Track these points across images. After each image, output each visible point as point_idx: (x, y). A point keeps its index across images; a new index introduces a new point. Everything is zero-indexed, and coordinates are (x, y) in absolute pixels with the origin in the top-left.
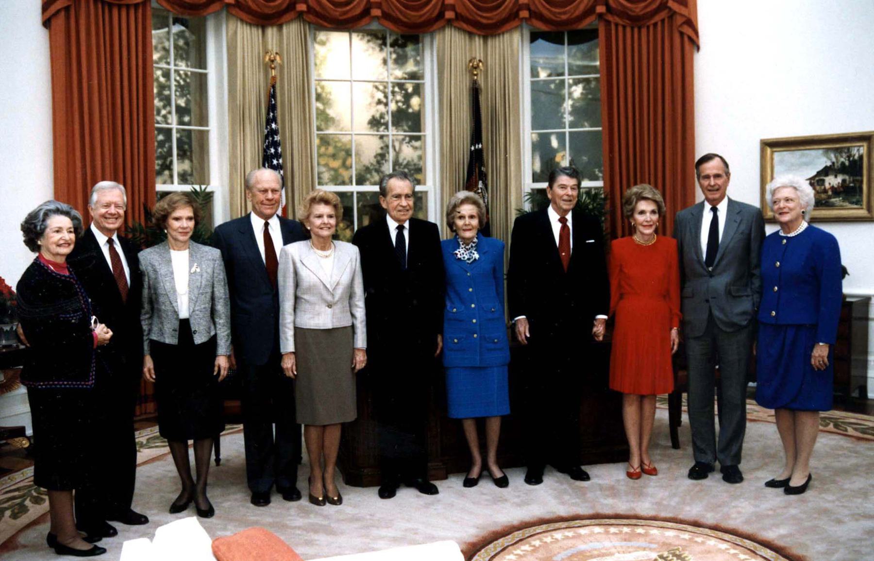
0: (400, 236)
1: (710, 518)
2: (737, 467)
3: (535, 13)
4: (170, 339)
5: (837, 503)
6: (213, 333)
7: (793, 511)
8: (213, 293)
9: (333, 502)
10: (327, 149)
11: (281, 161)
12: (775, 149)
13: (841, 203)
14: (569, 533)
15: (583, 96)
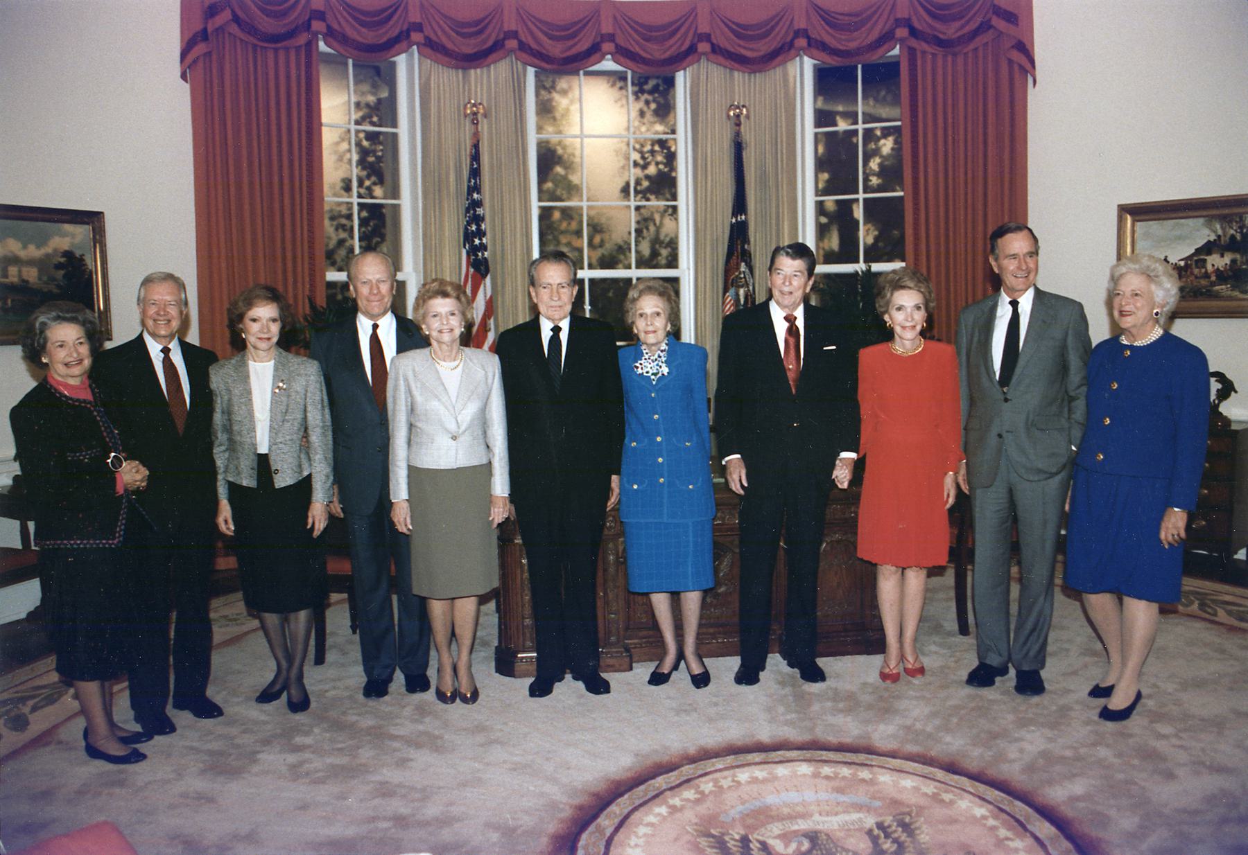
0: (555, 340)
1: (975, 757)
2: (1039, 673)
3: (816, 41)
4: (248, 480)
5: (1174, 741)
6: (306, 473)
7: (1103, 752)
8: (305, 419)
9: (465, 700)
10: (569, 224)
11: (484, 240)
12: (1137, 218)
13: (1229, 292)
14: (760, 773)
15: (894, 153)
